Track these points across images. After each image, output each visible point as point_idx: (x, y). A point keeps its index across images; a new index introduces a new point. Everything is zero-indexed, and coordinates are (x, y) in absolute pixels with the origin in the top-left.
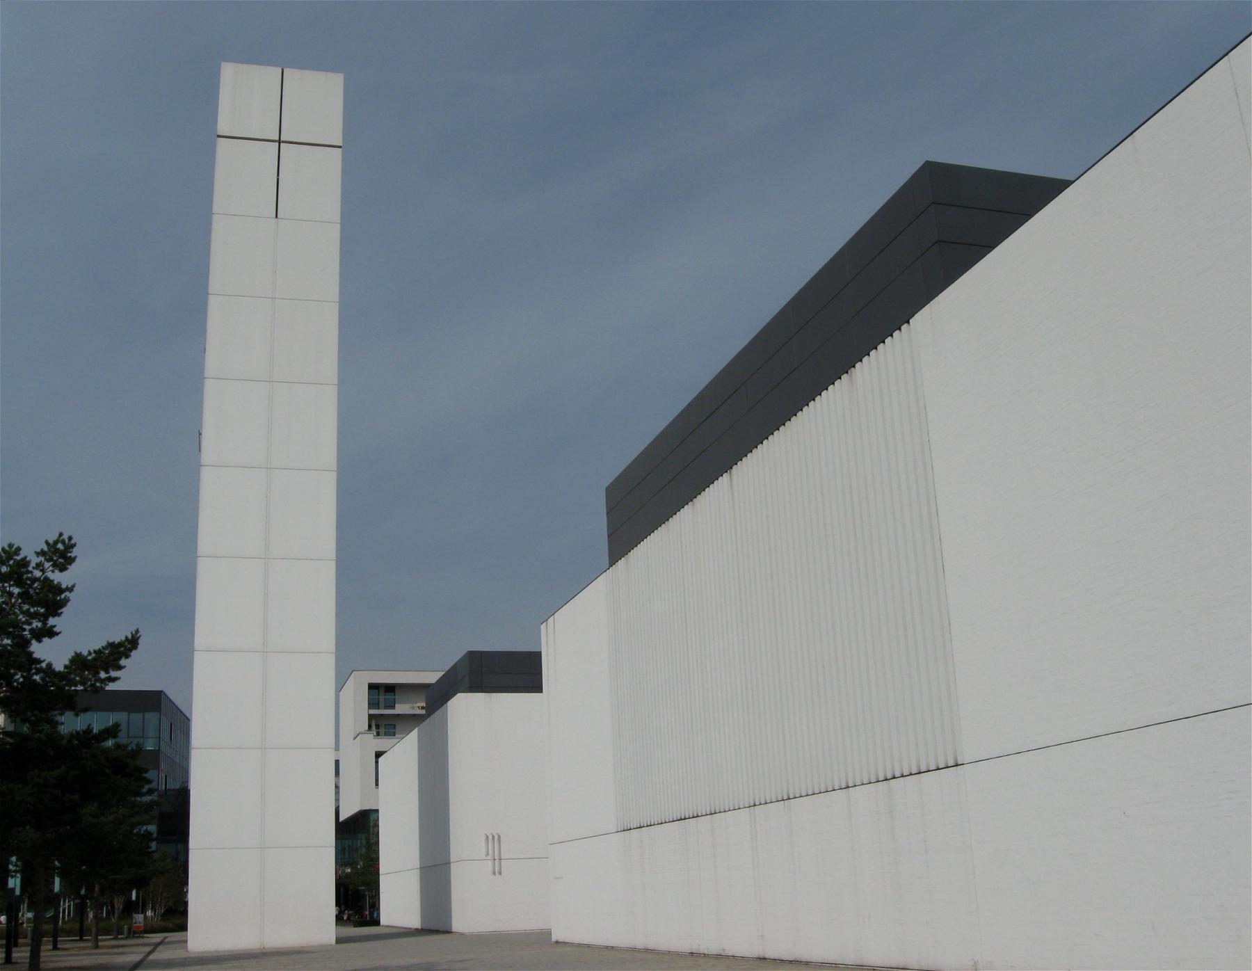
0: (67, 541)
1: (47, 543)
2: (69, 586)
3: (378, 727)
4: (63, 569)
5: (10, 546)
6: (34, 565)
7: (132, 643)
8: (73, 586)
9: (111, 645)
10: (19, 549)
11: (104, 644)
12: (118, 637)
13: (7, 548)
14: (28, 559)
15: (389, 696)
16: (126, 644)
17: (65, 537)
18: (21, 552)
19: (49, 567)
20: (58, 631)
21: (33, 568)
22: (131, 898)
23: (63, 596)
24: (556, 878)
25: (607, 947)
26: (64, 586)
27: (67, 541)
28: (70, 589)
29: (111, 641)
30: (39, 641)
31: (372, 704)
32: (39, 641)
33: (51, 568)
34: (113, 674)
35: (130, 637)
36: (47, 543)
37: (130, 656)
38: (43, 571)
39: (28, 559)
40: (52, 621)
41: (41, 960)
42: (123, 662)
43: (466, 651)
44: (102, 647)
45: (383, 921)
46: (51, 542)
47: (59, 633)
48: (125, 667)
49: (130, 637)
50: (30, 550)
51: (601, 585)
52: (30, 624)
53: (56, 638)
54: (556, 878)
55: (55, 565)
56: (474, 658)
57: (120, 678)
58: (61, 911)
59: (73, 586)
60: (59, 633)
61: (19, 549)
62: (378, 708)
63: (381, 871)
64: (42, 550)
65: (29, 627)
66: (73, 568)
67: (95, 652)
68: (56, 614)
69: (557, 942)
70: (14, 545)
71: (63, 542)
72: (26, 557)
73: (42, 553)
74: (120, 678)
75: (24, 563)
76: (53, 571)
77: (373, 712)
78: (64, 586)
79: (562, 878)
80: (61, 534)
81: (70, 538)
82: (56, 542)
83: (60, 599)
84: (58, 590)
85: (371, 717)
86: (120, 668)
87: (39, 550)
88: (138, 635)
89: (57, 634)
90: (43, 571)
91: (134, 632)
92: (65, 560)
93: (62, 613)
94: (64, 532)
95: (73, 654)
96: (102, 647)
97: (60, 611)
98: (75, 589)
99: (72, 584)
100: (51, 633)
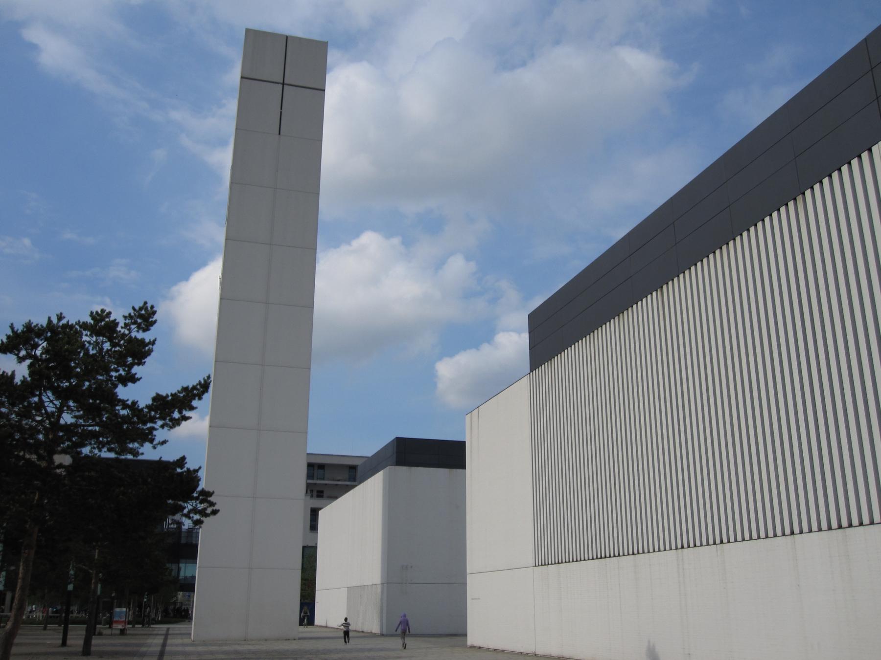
0: (149, 309)
1: (134, 308)
2: (152, 340)
3: (312, 491)
4: (146, 330)
5: (103, 311)
6: (123, 325)
7: (204, 387)
8: (155, 340)
9: (185, 389)
10: (110, 313)
11: (180, 389)
12: (191, 382)
13: (100, 313)
14: (117, 321)
15: (321, 471)
16: (198, 387)
17: (149, 305)
18: (111, 315)
19: (134, 329)
20: (139, 377)
21: (122, 328)
22: (102, 587)
23: (147, 348)
24: (473, 599)
25: (522, 653)
26: (147, 341)
27: (149, 309)
28: (153, 343)
29: (185, 386)
30: (125, 385)
31: (310, 476)
32: (125, 385)
33: (136, 329)
34: (187, 413)
35: (202, 382)
36: (134, 308)
37: (202, 398)
38: (129, 330)
39: (117, 321)
40: (136, 369)
41: (84, 637)
42: (195, 403)
43: (393, 437)
44: (178, 391)
45: (315, 624)
46: (137, 308)
47: (141, 378)
48: (196, 408)
49: (202, 382)
50: (118, 315)
51: (526, 380)
52: (117, 371)
53: (138, 383)
54: (473, 599)
55: (139, 327)
56: (401, 443)
57: (191, 418)
58: (130, 616)
59: (155, 340)
60: (141, 378)
61: (110, 313)
62: (313, 479)
63: (317, 588)
64: (130, 314)
65: (117, 374)
66: (153, 328)
67: (172, 395)
68: (140, 363)
69: (472, 647)
70: (105, 310)
71: (146, 309)
72: (115, 320)
73: (130, 316)
74: (191, 418)
75: (115, 324)
76: (138, 331)
77: (310, 481)
78: (147, 341)
79: (479, 599)
80: (146, 303)
81: (152, 307)
82: (141, 309)
83: (145, 351)
84: (142, 343)
85: (308, 485)
86: (192, 408)
87: (127, 315)
88: (209, 381)
89: (139, 379)
90: (129, 330)
91: (206, 378)
92: (77, 451)
93: (145, 362)
94: (148, 301)
95: (155, 395)
96: (178, 391)
97: (143, 361)
98: (156, 342)
99: (154, 338)
100: (133, 379)
